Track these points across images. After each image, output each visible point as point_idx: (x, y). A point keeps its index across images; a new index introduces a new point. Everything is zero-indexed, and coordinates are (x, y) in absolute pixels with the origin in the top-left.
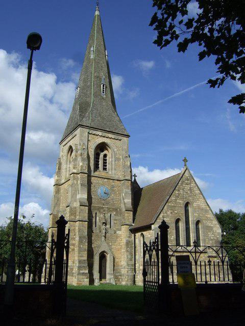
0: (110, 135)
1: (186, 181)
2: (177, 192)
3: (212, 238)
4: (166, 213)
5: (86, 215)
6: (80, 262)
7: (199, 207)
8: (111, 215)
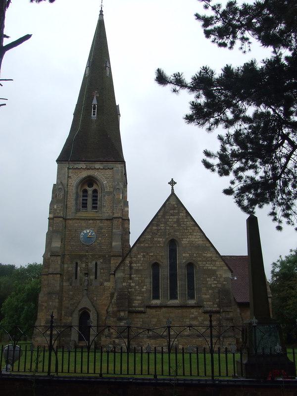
1: (171, 212)
3: (213, 286)
8: (96, 264)
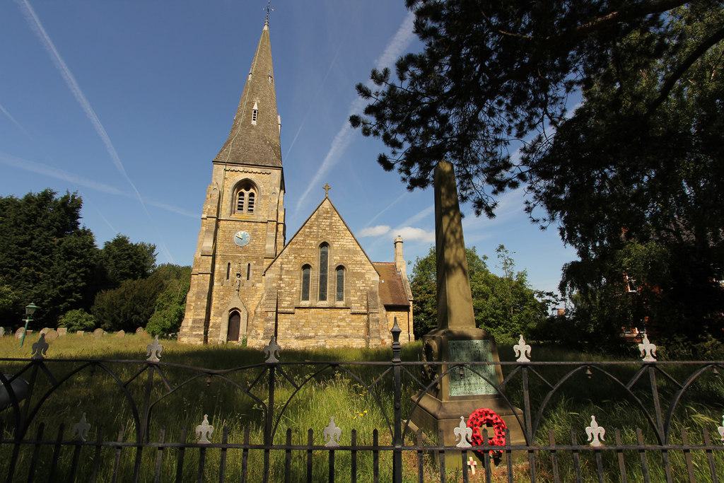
0: (255, 170)
1: (325, 215)
2: (308, 230)
4: (287, 257)
5: (210, 266)
6: (194, 321)
7: (342, 248)
8: (249, 265)
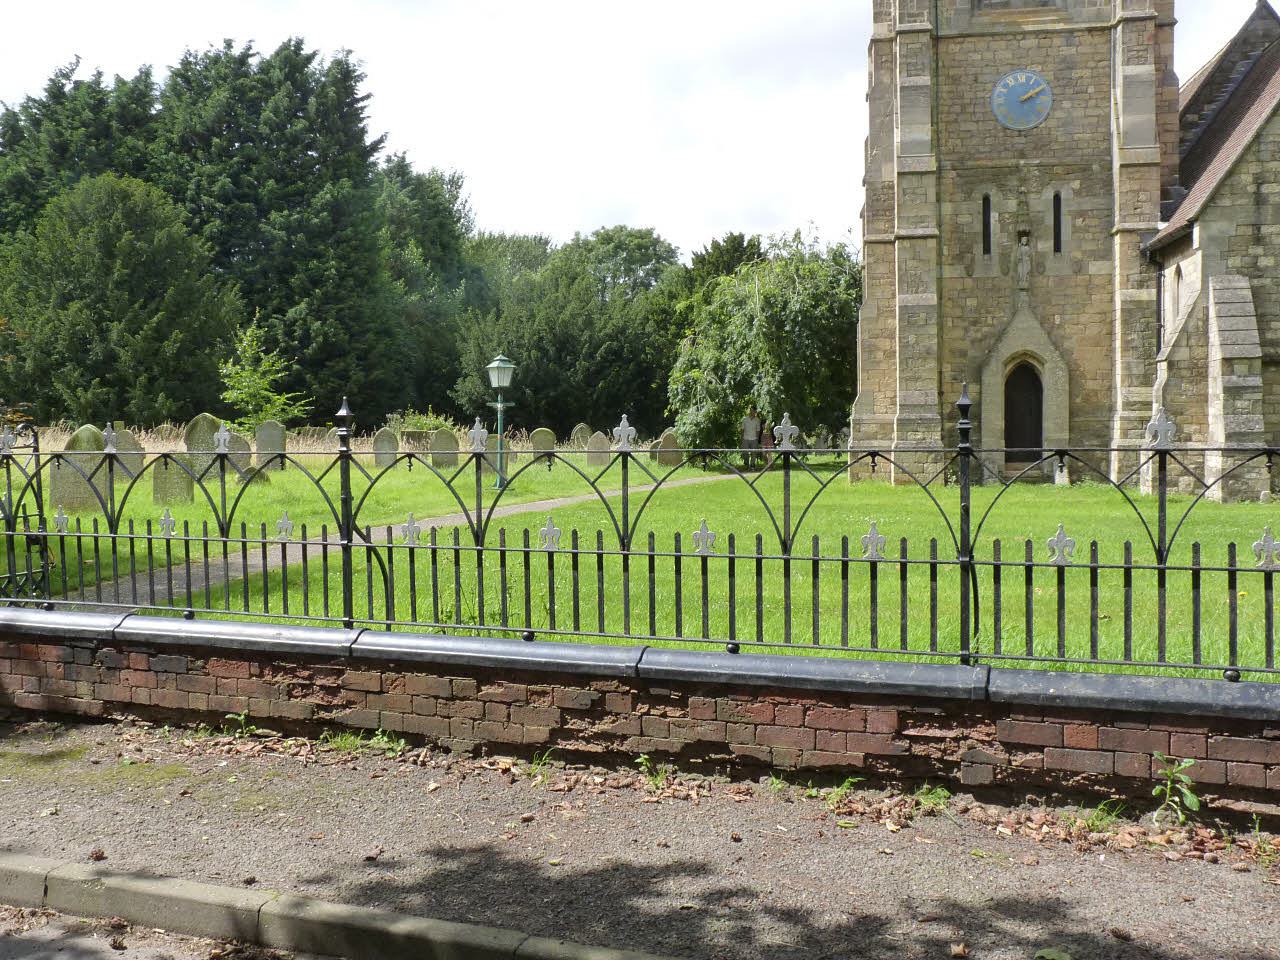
8: (1057, 198)
